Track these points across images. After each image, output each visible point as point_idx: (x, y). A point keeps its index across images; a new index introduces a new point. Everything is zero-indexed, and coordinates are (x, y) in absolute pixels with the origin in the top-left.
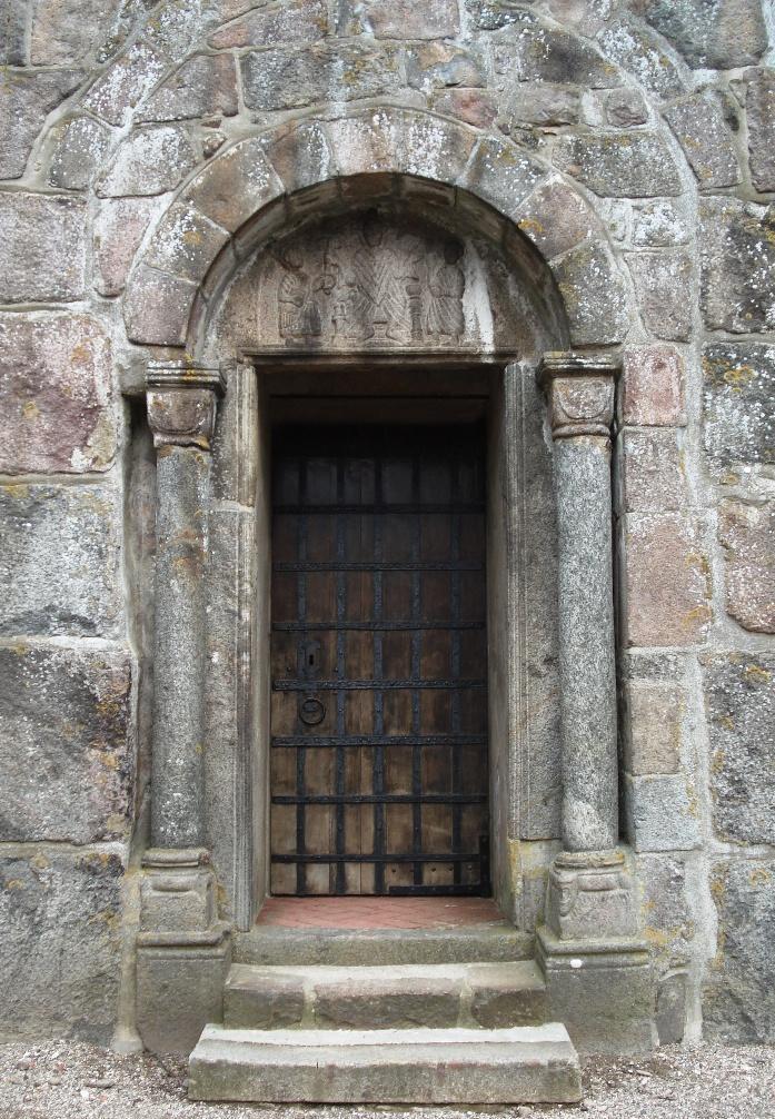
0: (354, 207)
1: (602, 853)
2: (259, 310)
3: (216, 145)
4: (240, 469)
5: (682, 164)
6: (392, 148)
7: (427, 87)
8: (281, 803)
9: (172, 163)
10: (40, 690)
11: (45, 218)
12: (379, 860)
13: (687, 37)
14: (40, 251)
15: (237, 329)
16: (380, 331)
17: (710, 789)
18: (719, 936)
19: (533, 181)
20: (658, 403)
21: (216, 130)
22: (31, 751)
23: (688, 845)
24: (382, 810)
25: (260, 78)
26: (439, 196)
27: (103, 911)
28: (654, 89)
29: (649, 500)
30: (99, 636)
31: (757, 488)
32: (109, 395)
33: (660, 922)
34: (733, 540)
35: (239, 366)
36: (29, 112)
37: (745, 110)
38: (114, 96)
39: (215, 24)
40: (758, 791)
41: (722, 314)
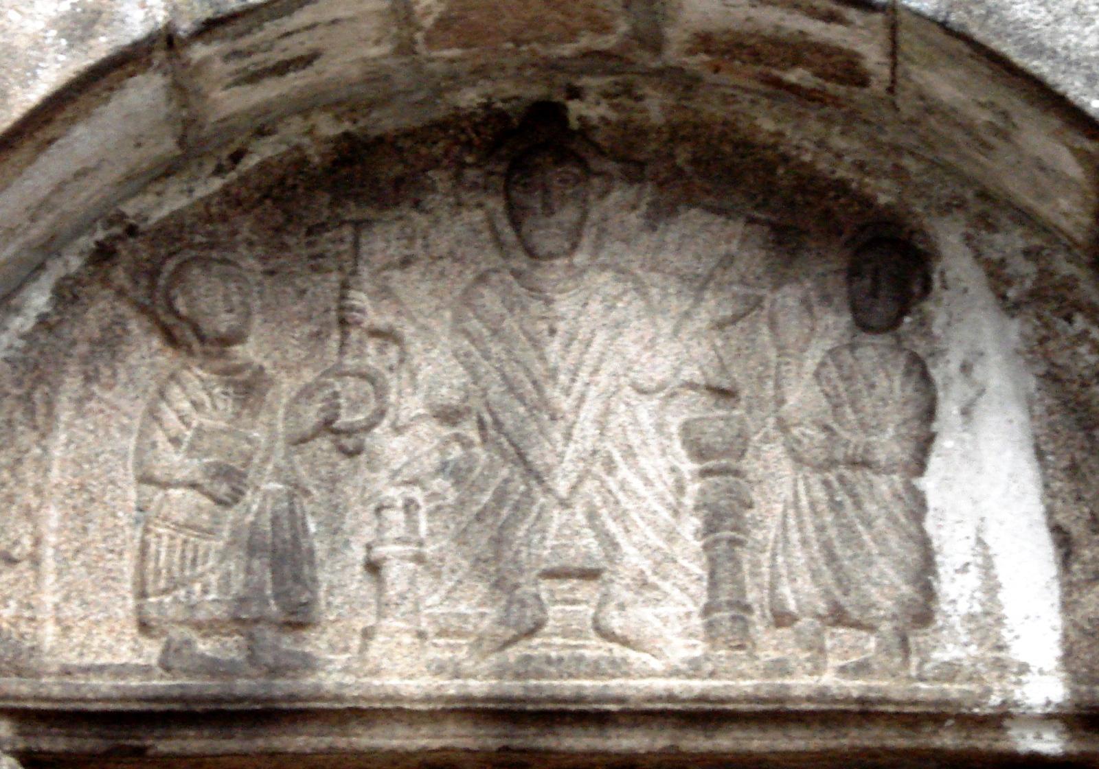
0: (469, 98)
2: (53, 517)
16: (568, 608)
26: (823, 50)
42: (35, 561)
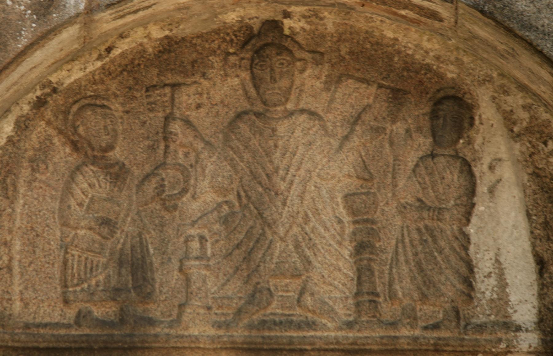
2: (17, 246)
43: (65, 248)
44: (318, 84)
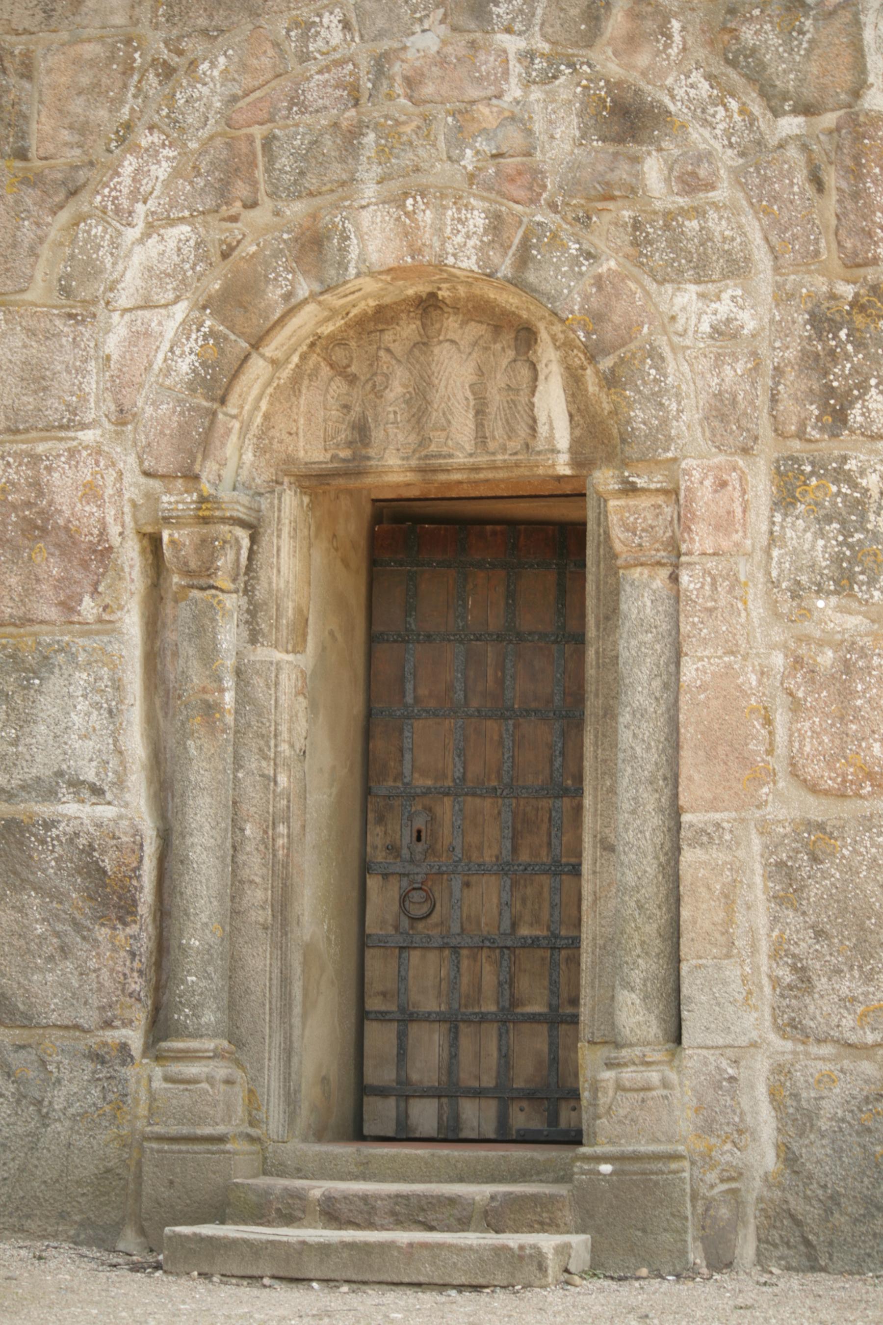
1: (647, 1050)
2: (302, 421)
3: (235, 243)
4: (277, 610)
5: (757, 238)
6: (427, 236)
7: (469, 159)
8: (377, 1020)
9: (187, 266)
10: (49, 862)
11: (53, 335)
12: (503, 1095)
13: (771, 79)
14: (48, 373)
15: (276, 446)
17: (770, 977)
18: (777, 1147)
19: (584, 268)
20: (717, 528)
21: (234, 225)
22: (40, 929)
23: (743, 1041)
24: (507, 1032)
25: (284, 161)
27: (111, 1102)
28: (731, 145)
29: (705, 642)
30: (109, 803)
31: (832, 625)
32: (121, 534)
33: (708, 1128)
34: (799, 687)
35: (278, 488)
36: (35, 214)
37: (833, 167)
38: (125, 191)
39: (234, 99)
40: (824, 980)
41: (795, 419)
42: (297, 434)
43: (325, 421)
44: (457, 325)
